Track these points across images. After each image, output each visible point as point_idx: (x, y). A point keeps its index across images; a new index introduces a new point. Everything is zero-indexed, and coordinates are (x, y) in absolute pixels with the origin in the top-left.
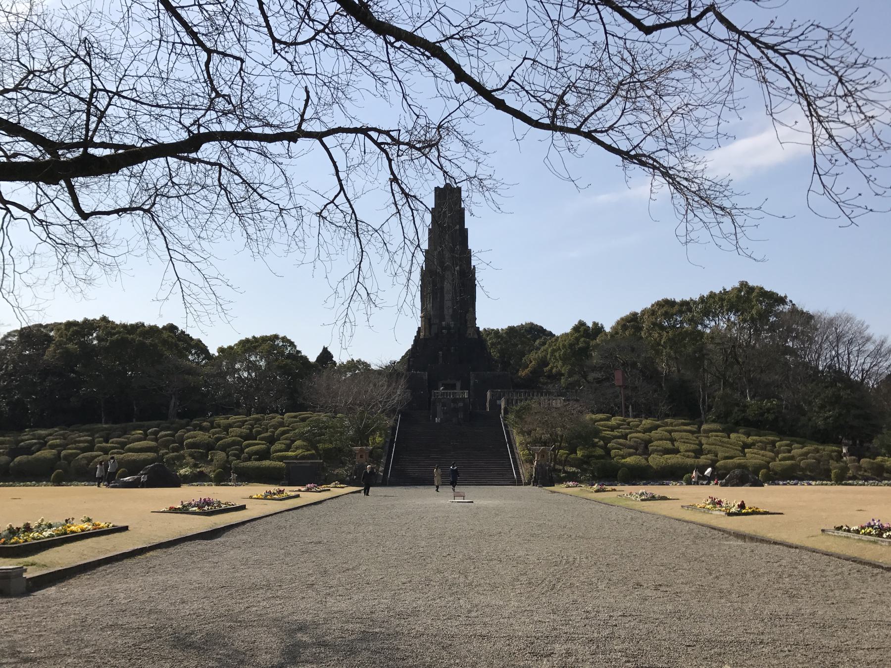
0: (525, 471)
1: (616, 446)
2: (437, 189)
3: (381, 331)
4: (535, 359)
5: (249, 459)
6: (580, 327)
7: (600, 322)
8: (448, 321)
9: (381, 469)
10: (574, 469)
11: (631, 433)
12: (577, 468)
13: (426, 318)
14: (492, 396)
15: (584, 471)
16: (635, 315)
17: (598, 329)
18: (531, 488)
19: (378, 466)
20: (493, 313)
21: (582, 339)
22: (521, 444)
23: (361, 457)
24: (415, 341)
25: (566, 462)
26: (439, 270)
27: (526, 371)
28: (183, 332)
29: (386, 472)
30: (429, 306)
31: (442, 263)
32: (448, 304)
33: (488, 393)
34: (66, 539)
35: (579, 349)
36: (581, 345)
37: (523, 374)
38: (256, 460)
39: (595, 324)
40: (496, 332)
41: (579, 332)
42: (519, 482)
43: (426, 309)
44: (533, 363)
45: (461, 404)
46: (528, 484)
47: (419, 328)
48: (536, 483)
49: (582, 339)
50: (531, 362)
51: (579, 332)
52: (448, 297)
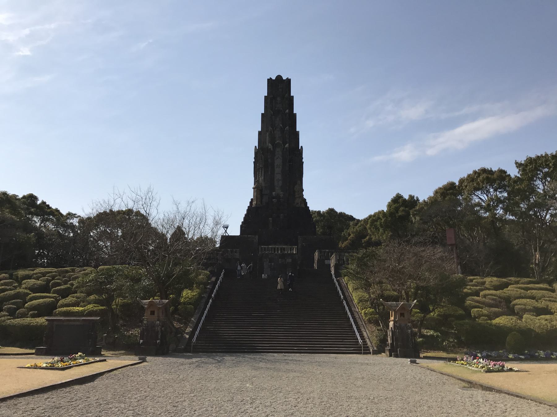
0: (370, 334)
1: (474, 304)
2: (270, 81)
3: (214, 198)
4: (353, 233)
5: (24, 315)
6: (398, 200)
7: (416, 195)
8: (278, 191)
9: (189, 330)
10: (431, 332)
11: (482, 290)
12: (435, 331)
13: (258, 189)
14: (320, 256)
15: (445, 335)
16: (451, 186)
17: (413, 202)
18: (384, 359)
19: (186, 325)
20: (318, 195)
21: (402, 208)
22: (360, 301)
23: (153, 313)
24: (248, 210)
25: (422, 324)
26: (270, 146)
27: (346, 243)
28: (43, 203)
29: (192, 334)
30: (261, 179)
31: (272, 141)
32: (278, 176)
33: (316, 254)
34: (116, 355)
35: (400, 216)
36: (400, 214)
37: (343, 246)
38: (33, 316)
39: (411, 197)
40: (319, 212)
41: (398, 203)
42: (364, 350)
43: (258, 181)
44: (352, 235)
45: (290, 260)
46: (379, 351)
47: (252, 199)
48: (394, 353)
49: (402, 208)
50: (349, 235)
51: (398, 203)
52: (278, 170)
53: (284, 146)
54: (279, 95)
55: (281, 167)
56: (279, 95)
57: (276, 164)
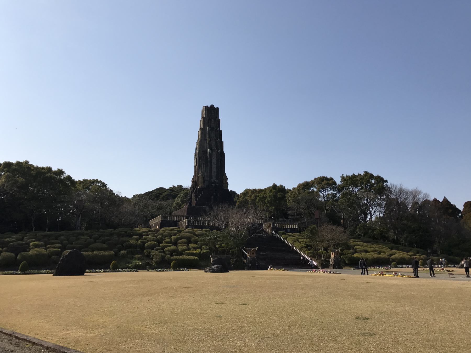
54: (211, 116)
56: (211, 116)
57: (213, 162)
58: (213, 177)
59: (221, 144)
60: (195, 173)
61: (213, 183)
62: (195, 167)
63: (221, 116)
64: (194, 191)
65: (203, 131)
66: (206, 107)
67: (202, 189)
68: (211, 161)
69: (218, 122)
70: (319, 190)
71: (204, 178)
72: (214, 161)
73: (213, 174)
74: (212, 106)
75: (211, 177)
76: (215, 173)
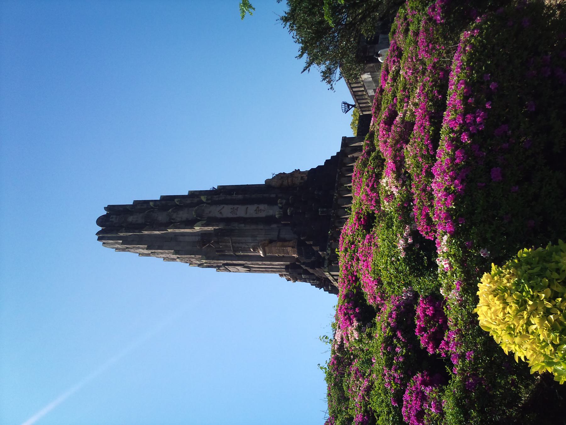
53: (203, 203)
54: (125, 225)
55: (236, 207)
56: (125, 225)
57: (230, 215)
58: (271, 213)
59: (195, 196)
60: (266, 270)
61: (285, 213)
62: (250, 269)
63: (126, 199)
64: (311, 271)
65: (155, 245)
66: (101, 236)
67: (300, 246)
68: (227, 221)
69: (141, 206)
70: (550, 321)
71: (271, 242)
72: (227, 211)
73: (263, 215)
74: (101, 221)
75: (269, 220)
76: (262, 207)
